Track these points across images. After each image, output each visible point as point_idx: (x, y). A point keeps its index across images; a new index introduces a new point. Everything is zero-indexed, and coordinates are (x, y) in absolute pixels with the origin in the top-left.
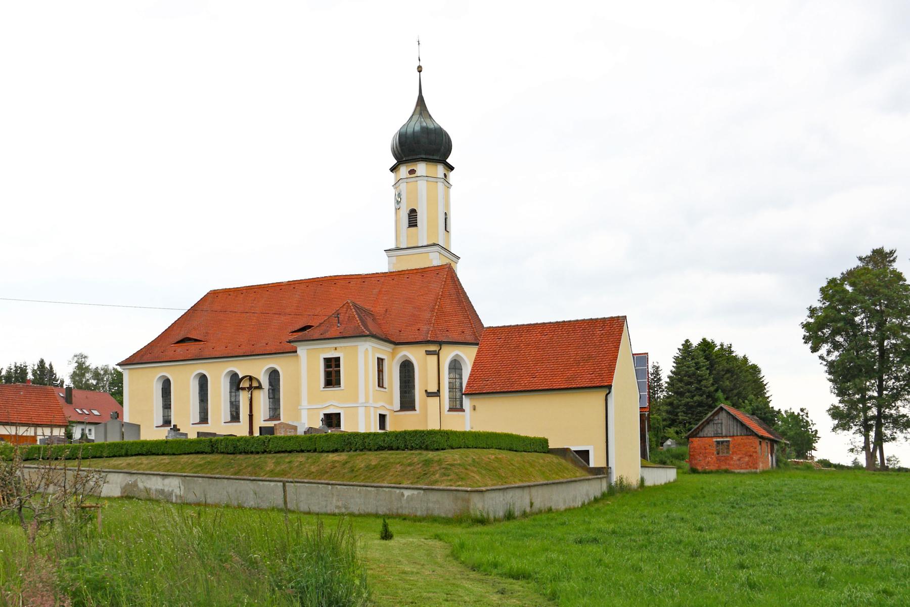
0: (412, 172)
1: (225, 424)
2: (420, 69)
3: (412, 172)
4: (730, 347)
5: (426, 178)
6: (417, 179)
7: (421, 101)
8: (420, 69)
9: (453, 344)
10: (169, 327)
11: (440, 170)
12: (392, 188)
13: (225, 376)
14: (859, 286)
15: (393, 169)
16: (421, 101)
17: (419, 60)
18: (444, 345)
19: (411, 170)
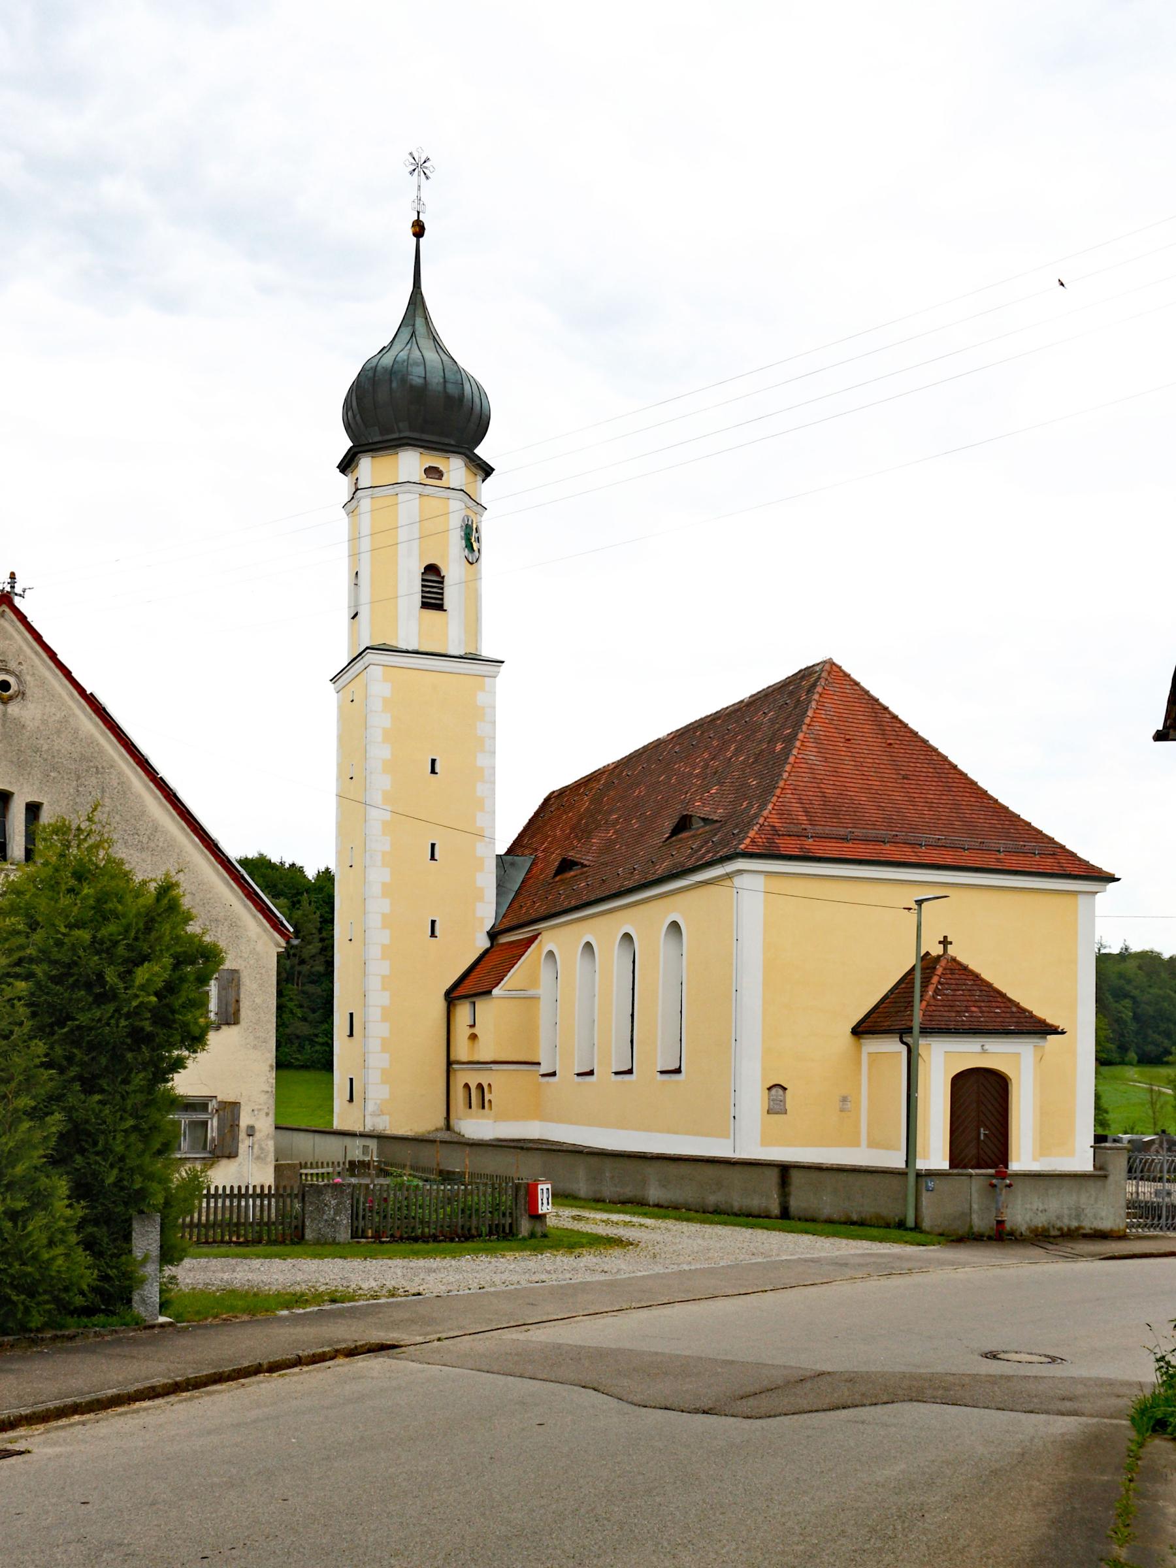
0: (433, 472)
1: (580, 1079)
2: (419, 230)
3: (433, 472)
4: (1126, 949)
5: (420, 488)
6: (398, 489)
7: (417, 301)
8: (419, 230)
9: (560, 927)
10: (519, 835)
11: (455, 469)
12: (343, 513)
13: (582, 954)
14: (106, 878)
15: (347, 465)
16: (417, 301)
17: (1062, 284)
18: (501, 936)
19: (430, 467)
